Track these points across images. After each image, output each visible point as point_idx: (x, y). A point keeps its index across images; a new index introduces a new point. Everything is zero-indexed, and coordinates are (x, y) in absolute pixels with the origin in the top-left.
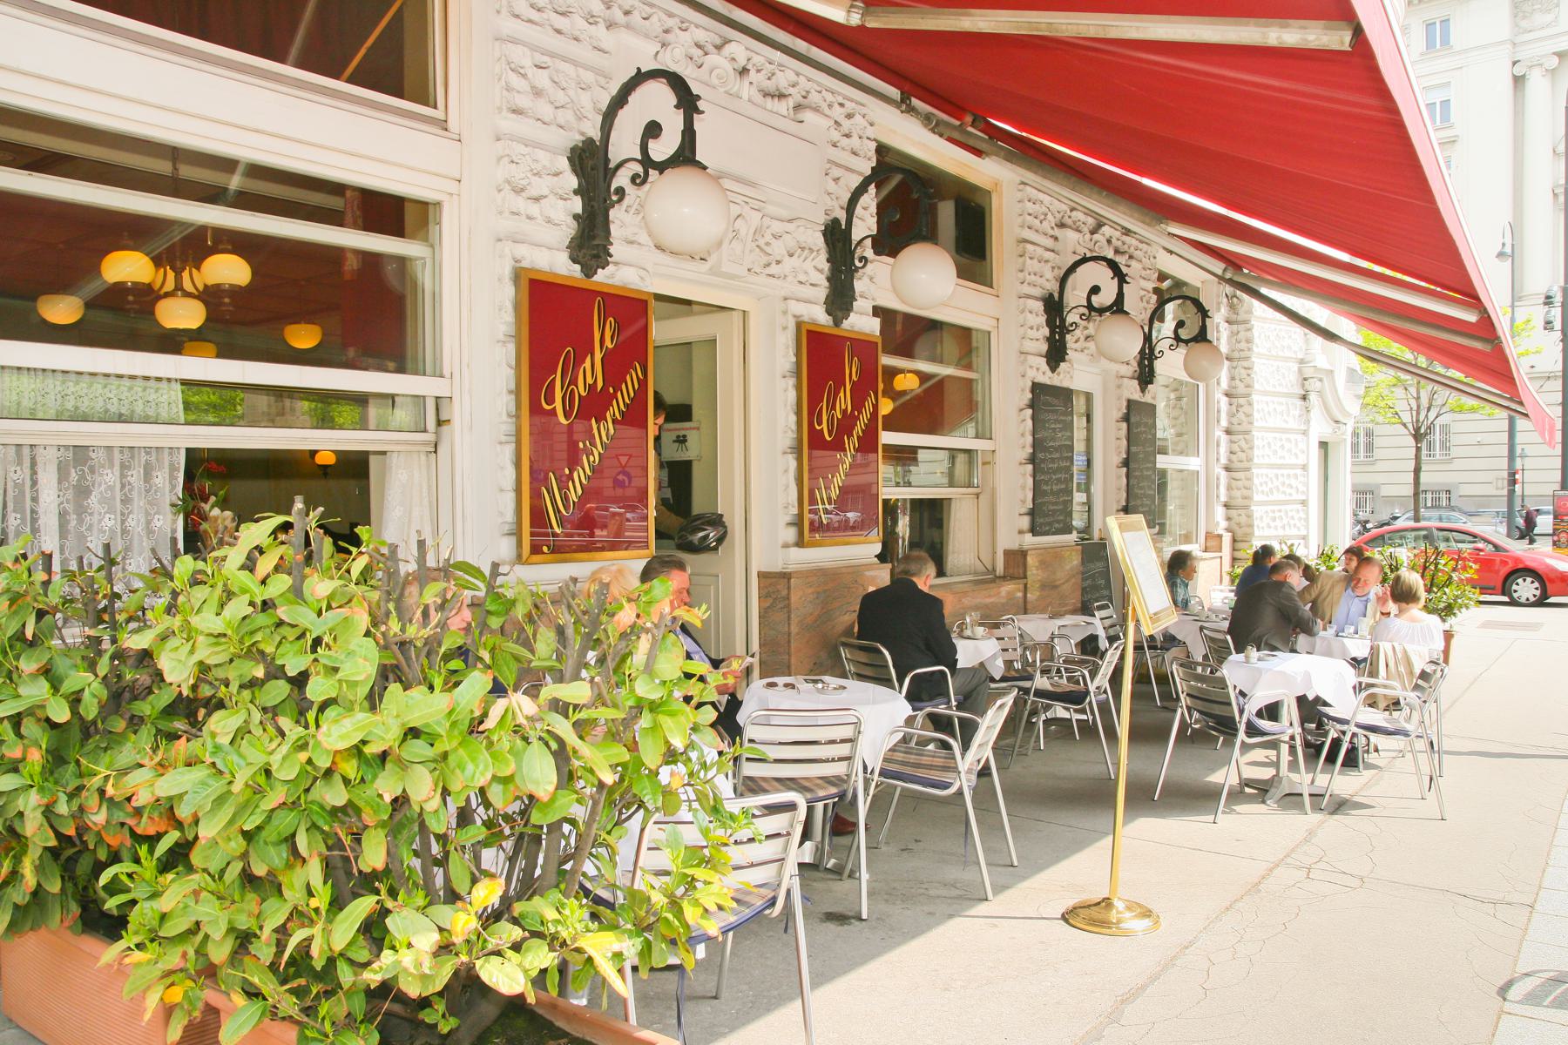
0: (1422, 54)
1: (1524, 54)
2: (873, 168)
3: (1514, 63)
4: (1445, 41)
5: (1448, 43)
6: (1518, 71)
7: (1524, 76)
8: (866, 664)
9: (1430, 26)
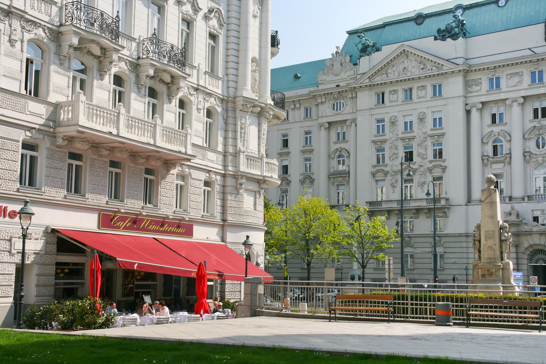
0: (529, 85)
1: (471, 101)
2: (173, 310)
3: (466, 104)
4: (440, 93)
5: (499, 87)
6: (468, 108)
7: (470, 110)
8: (93, 73)
9: (434, 87)
